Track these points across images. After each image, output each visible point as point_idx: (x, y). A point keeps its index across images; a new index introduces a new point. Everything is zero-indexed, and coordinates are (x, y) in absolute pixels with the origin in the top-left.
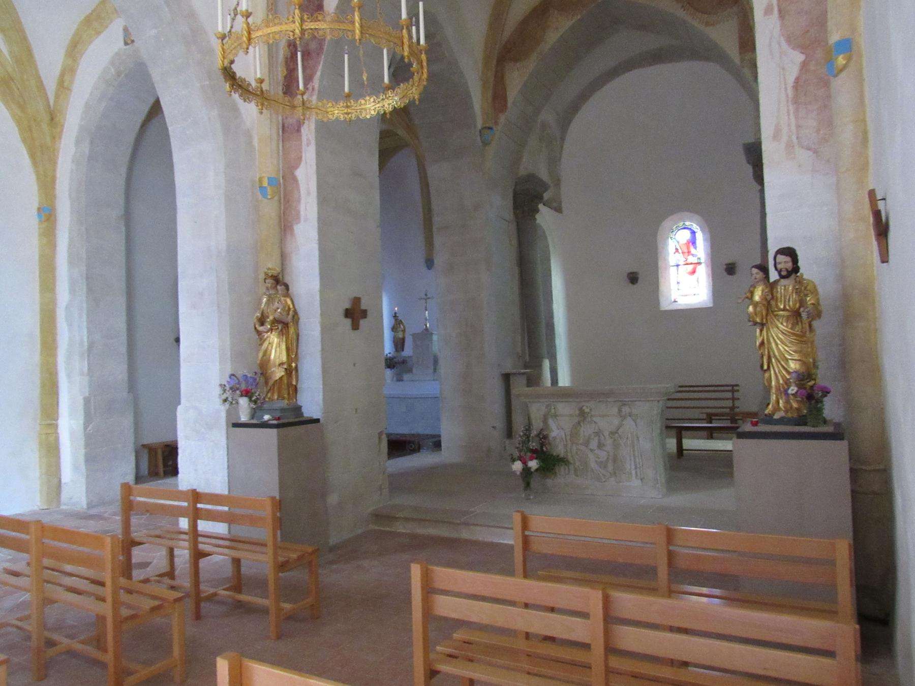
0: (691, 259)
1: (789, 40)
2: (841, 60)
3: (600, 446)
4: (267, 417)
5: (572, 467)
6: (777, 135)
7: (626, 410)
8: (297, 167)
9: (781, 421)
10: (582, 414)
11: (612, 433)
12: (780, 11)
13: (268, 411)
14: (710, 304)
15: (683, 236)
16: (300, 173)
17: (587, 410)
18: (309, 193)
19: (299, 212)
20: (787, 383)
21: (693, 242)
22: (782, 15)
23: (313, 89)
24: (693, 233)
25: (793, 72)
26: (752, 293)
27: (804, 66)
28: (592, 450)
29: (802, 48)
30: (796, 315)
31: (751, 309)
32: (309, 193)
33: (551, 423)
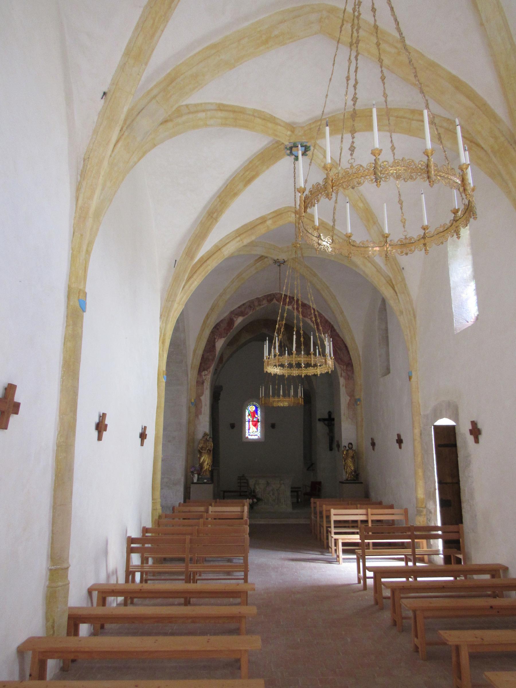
0: (255, 419)
1: (347, 394)
2: (358, 403)
3: (273, 494)
4: (205, 481)
5: (263, 501)
6: (344, 414)
7: (282, 482)
8: (201, 396)
9: (350, 480)
10: (268, 484)
11: (277, 490)
12: (345, 386)
13: (205, 479)
14: (263, 440)
15: (252, 408)
16: (202, 398)
17: (269, 482)
18: (206, 405)
19: (201, 411)
20: (352, 472)
21: (256, 411)
22: (346, 387)
23: (210, 371)
24: (256, 408)
25: (348, 401)
26: (343, 452)
27: (350, 400)
28: (270, 496)
29: (350, 396)
30: (353, 457)
31: (344, 455)
32: (206, 405)
33: (257, 487)
